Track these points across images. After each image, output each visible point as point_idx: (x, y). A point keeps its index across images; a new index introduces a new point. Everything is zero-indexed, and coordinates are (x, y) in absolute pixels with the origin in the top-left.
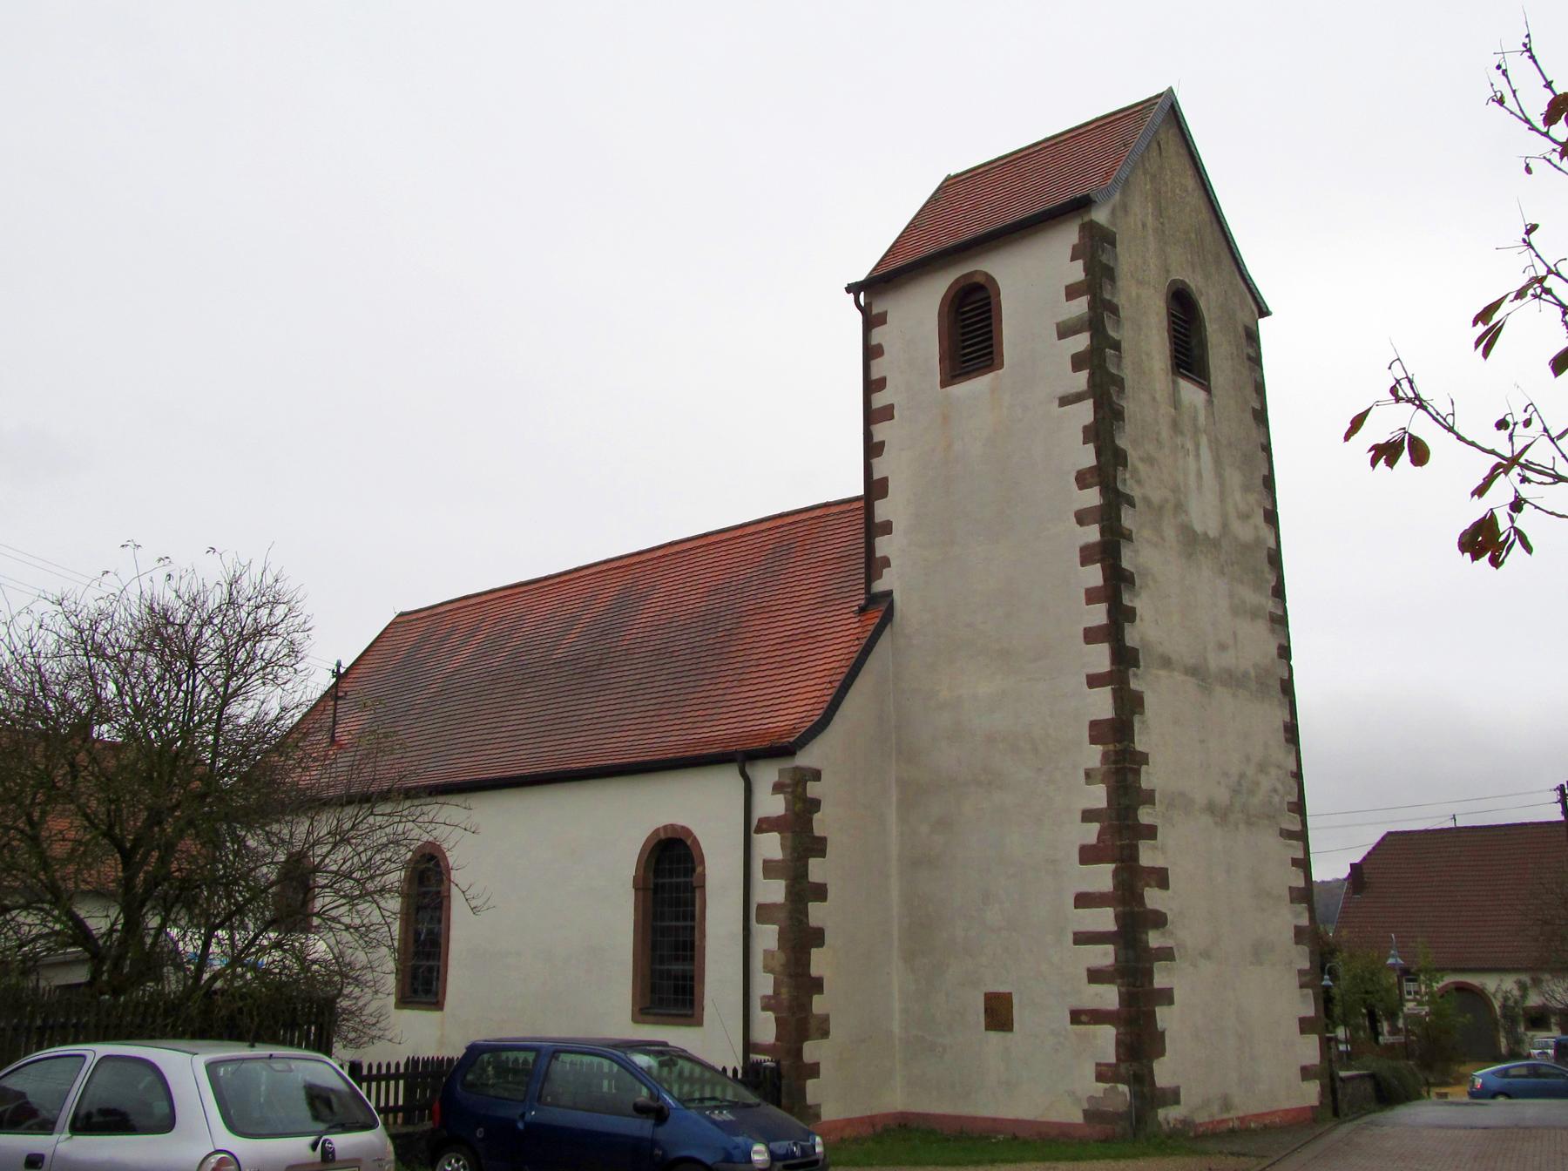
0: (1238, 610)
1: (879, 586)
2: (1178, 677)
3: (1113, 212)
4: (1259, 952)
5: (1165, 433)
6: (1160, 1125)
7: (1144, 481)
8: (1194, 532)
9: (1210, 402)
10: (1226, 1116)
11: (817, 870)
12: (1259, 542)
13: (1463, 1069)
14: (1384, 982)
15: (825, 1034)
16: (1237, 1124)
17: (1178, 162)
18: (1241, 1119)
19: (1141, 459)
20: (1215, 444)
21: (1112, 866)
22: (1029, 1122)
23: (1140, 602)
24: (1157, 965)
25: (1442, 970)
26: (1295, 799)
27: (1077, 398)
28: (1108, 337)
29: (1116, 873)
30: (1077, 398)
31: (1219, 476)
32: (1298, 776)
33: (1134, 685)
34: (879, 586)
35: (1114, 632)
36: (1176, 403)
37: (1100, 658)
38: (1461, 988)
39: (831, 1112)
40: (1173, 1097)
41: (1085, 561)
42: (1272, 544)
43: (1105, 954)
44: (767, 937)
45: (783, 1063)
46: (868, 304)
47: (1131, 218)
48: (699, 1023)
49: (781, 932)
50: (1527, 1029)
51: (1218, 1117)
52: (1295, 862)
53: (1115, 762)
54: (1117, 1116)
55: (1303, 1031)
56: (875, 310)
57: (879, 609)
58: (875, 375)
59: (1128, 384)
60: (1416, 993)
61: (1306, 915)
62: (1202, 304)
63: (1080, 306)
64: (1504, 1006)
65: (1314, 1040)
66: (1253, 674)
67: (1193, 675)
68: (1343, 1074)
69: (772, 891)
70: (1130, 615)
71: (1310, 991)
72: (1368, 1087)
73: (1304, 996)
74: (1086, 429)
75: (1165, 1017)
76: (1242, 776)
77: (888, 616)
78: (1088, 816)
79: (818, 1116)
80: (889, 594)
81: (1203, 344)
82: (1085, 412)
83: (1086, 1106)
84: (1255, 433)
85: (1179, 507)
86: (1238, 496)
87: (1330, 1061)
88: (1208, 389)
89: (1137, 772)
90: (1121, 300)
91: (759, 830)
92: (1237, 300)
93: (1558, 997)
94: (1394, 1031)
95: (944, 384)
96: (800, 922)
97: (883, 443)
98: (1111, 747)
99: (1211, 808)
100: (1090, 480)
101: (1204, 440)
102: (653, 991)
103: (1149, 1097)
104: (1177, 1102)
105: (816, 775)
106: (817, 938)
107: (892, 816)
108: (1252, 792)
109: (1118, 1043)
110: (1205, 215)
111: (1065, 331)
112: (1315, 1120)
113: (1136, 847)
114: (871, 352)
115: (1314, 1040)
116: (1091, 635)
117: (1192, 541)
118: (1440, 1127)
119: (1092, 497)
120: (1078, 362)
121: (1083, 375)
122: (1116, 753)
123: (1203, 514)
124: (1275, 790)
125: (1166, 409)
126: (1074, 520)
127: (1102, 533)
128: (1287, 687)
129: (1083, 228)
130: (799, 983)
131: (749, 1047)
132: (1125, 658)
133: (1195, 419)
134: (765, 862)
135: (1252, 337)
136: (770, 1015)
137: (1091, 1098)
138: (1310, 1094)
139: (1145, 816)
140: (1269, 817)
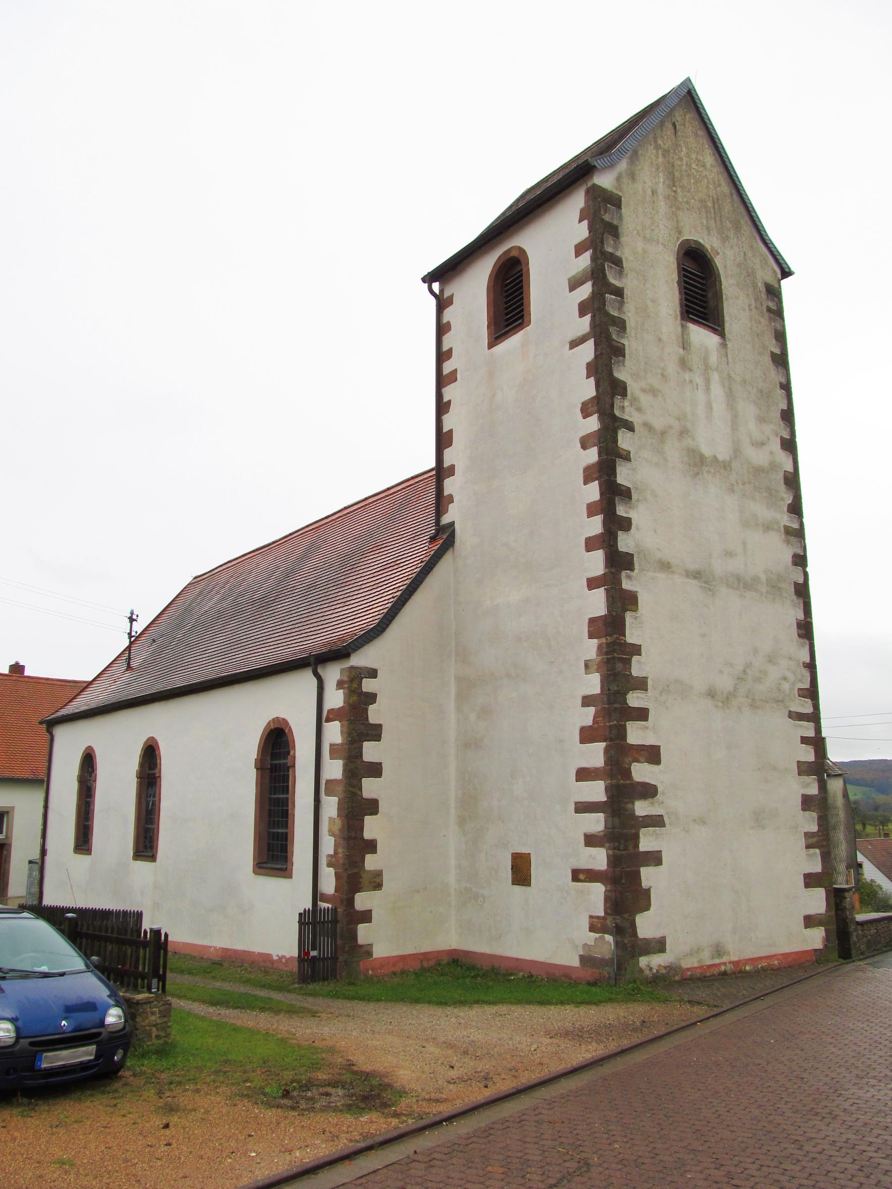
1: (446, 520)
2: (679, 579)
3: (619, 179)
4: (760, 818)
5: (672, 368)
6: (641, 970)
7: (640, 407)
9: (724, 345)
10: (717, 961)
12: (773, 466)
15: (378, 886)
16: (729, 967)
18: (736, 963)
19: (643, 390)
20: (728, 381)
22: (541, 963)
24: (643, 831)
26: (807, 685)
27: (582, 340)
28: (609, 285)
29: (606, 751)
30: (582, 340)
32: (811, 666)
33: (626, 585)
34: (446, 520)
36: (685, 344)
37: (596, 563)
39: (380, 951)
41: (587, 480)
42: (790, 469)
43: (598, 821)
44: (331, 806)
45: (340, 910)
46: (442, 291)
48: (290, 876)
49: (339, 803)
53: (607, 653)
55: (807, 885)
57: (444, 538)
59: (631, 323)
61: (816, 785)
62: (718, 262)
63: (585, 260)
66: (763, 577)
67: (695, 578)
69: (334, 769)
70: (626, 524)
71: (817, 851)
75: (648, 876)
76: (749, 665)
78: (587, 701)
79: (369, 954)
80: (452, 524)
82: (588, 351)
83: (582, 953)
84: (775, 376)
85: (684, 433)
86: (752, 425)
88: (721, 334)
89: (628, 662)
92: (757, 261)
95: (491, 345)
97: (449, 402)
98: (604, 640)
99: (711, 694)
100: (591, 410)
101: (715, 377)
102: (269, 850)
103: (631, 946)
105: (373, 673)
106: (372, 807)
107: (451, 706)
109: (607, 899)
111: (574, 285)
112: (818, 962)
114: (442, 329)
117: (698, 463)
119: (593, 424)
121: (588, 318)
122: (608, 644)
123: (712, 439)
124: (785, 679)
126: (579, 445)
128: (802, 591)
129: (587, 192)
130: (355, 846)
132: (619, 562)
133: (705, 359)
134: (331, 745)
135: (774, 293)
136: (331, 870)
137: (585, 945)
138: (816, 938)
139: (634, 700)
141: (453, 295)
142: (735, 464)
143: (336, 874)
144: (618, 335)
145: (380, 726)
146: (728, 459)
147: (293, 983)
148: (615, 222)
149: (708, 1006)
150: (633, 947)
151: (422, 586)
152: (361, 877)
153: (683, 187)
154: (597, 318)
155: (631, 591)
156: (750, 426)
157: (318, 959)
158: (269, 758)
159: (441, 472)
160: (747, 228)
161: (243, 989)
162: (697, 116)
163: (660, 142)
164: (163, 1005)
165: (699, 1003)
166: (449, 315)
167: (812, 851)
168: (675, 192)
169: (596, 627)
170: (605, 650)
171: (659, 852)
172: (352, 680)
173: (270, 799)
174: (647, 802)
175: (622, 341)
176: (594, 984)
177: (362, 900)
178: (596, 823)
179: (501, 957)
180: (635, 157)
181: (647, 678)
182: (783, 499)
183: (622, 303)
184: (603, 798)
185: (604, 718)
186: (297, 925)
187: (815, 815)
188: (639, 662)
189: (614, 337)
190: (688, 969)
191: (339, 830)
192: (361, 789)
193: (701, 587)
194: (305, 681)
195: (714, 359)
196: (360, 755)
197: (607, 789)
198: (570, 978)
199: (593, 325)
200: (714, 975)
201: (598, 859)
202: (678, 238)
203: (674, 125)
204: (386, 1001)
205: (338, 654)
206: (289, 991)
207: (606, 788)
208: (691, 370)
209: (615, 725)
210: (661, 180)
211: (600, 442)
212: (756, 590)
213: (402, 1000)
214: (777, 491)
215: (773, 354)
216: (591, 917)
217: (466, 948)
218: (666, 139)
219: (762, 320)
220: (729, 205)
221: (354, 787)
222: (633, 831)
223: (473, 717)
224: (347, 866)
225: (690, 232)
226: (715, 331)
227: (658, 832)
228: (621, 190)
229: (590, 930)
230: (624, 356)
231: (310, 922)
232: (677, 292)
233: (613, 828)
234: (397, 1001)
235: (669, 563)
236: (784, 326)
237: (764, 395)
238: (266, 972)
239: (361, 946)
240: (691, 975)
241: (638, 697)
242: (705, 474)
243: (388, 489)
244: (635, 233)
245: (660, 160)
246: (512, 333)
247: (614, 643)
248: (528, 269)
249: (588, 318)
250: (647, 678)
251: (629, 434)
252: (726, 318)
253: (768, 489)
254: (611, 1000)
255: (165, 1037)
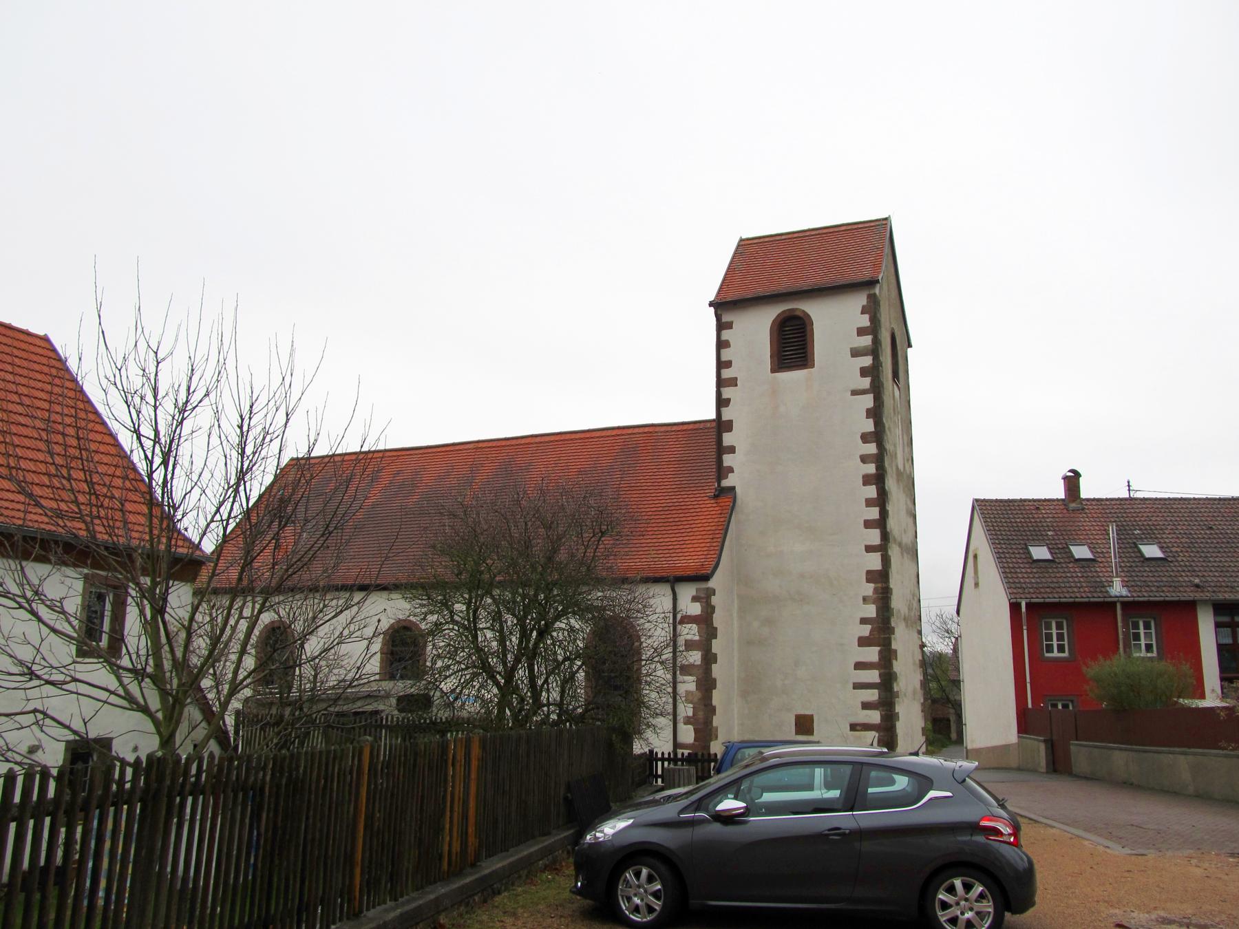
1: (725, 483)
29: (880, 652)
178: (873, 695)
184: (878, 680)
223: (756, 624)
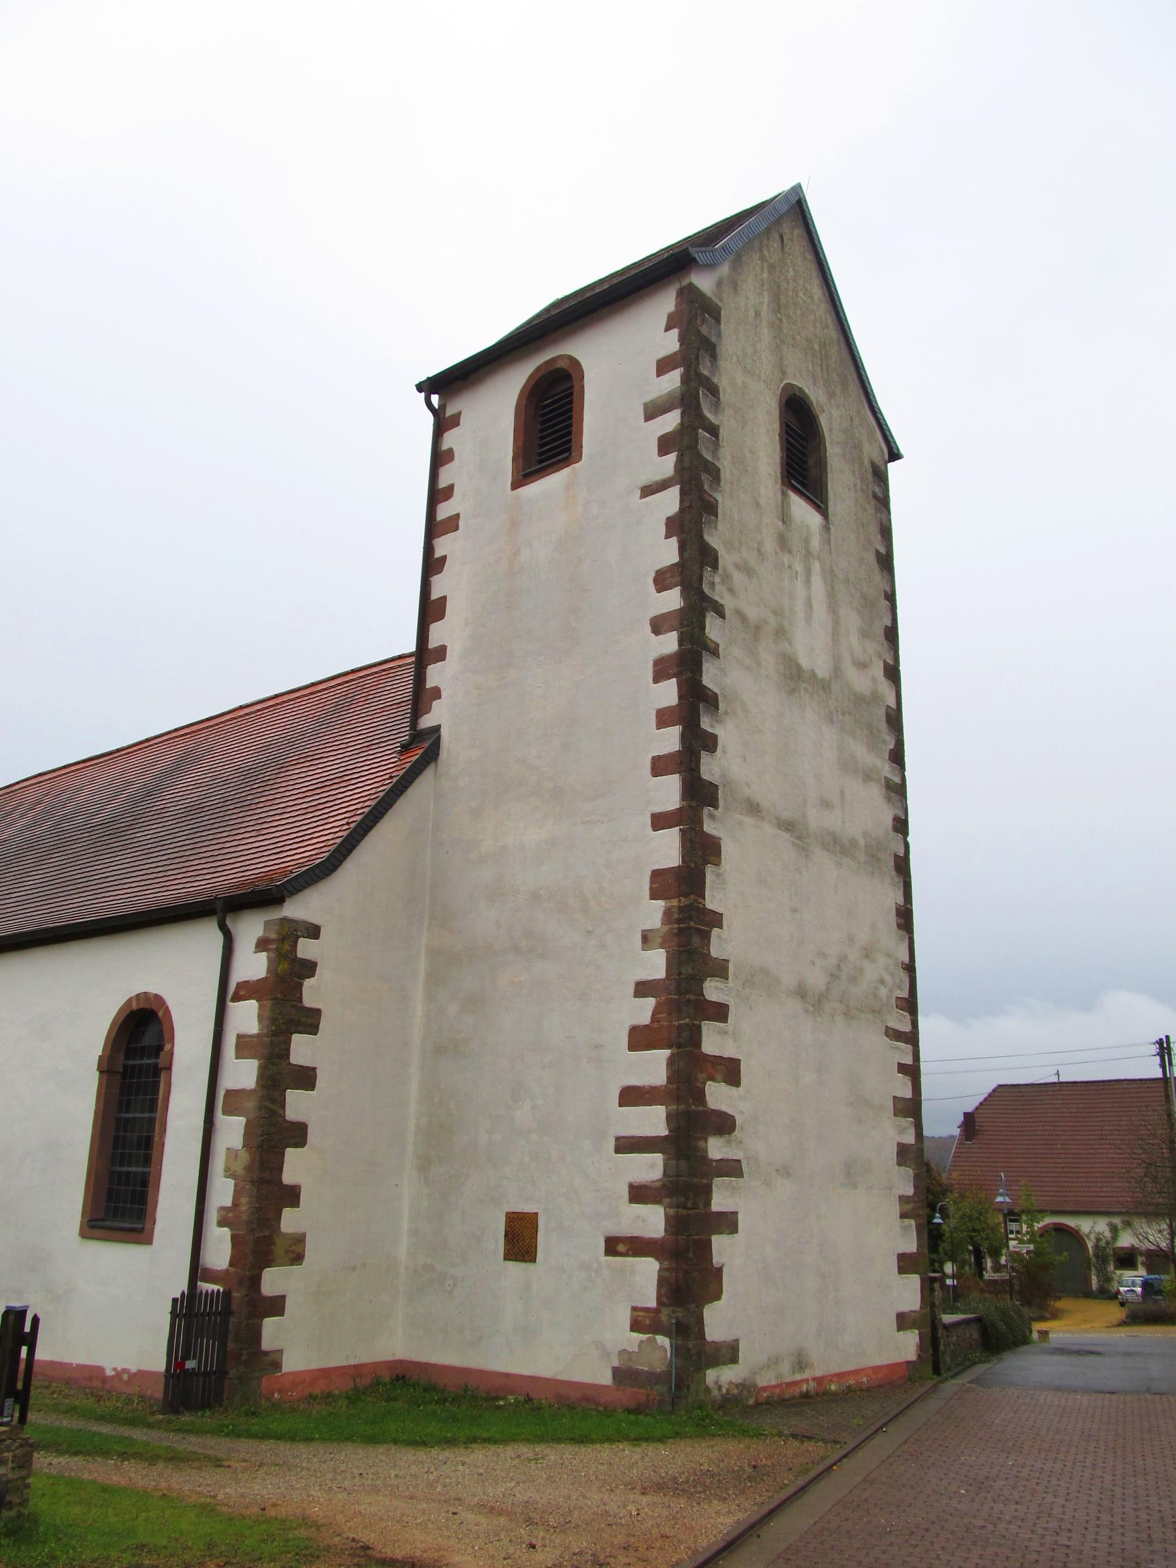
0: (847, 766)
1: (426, 722)
2: (769, 829)
3: (719, 284)
4: (852, 1173)
5: (770, 545)
6: (708, 1390)
7: (738, 590)
8: (799, 666)
9: (826, 528)
10: (798, 1377)
11: (302, 1049)
12: (876, 697)
13: (1059, 1304)
14: (990, 1222)
15: (298, 1258)
17: (797, 246)
18: (819, 1380)
19: (737, 566)
20: (830, 575)
21: (667, 1053)
23: (725, 731)
24: (717, 1181)
25: (1042, 1211)
29: (671, 1062)
31: (833, 608)
32: (910, 968)
33: (709, 827)
34: (426, 722)
35: (689, 761)
36: (785, 517)
37: (668, 792)
38: (1060, 1229)
39: (294, 1361)
40: (729, 1353)
41: (658, 677)
42: (892, 702)
43: (653, 1166)
44: (232, 1131)
45: (235, 1294)
46: (443, 406)
47: (745, 305)
48: (149, 1241)
49: (248, 1126)
50: (1116, 1268)
51: (789, 1379)
52: (902, 1068)
53: (679, 921)
54: (652, 1378)
55: (902, 1270)
56: (450, 412)
57: (423, 748)
58: (442, 483)
59: (726, 475)
60: (1018, 1232)
61: (912, 1131)
62: (823, 420)
63: (673, 380)
64: (1096, 1247)
65: (914, 1280)
66: (862, 842)
67: (787, 830)
68: (947, 1318)
69: (242, 1074)
70: (710, 743)
71: (913, 1222)
72: (974, 1333)
73: (905, 1228)
74: (670, 522)
75: (722, 1247)
76: (843, 958)
77: (432, 755)
78: (643, 989)
79: (277, 1365)
80: (437, 729)
81: (822, 464)
82: (670, 502)
83: (616, 1364)
84: (878, 578)
85: (781, 633)
87: (933, 1305)
89: (706, 936)
90: (723, 382)
91: (237, 998)
93: (1151, 1238)
94: (997, 1268)
95: (516, 485)
96: (273, 1113)
98: (675, 902)
99: (801, 993)
101: (816, 567)
102: (109, 1199)
103: (696, 1352)
104: (734, 1360)
105: (314, 932)
106: (298, 1134)
107: (418, 991)
108: (853, 980)
109: (661, 1282)
110: (833, 333)
111: (652, 411)
113: (699, 1028)
114: (440, 458)
115: (914, 1280)
116: (660, 766)
117: (794, 676)
118: (1058, 1389)
120: (665, 445)
121: (672, 458)
122: (681, 909)
123: (812, 648)
124: (882, 982)
125: (771, 521)
127: (681, 642)
128: (902, 866)
129: (680, 293)
131: (197, 1271)
132: (700, 794)
133: (807, 541)
134: (239, 1037)
135: (881, 477)
138: (907, 1345)
139: (713, 991)
140: (873, 1011)
141: (460, 414)
142: (835, 687)
143: (233, 1237)
144: (711, 486)
145: (318, 1011)
146: (827, 677)
147: (153, 1413)
148: (713, 339)
149: (825, 1441)
150: (699, 1355)
151: (390, 812)
152: (274, 1244)
153: (788, 316)
154: (686, 460)
155: (713, 837)
156: (853, 641)
157: (197, 1374)
158: (121, 1056)
159: (425, 654)
160: (854, 387)
161: (77, 1424)
162: (805, 234)
163: (765, 253)
164: (21, 1446)
165: (810, 1438)
166: (450, 439)
167: (907, 1221)
168: (780, 320)
169: (662, 883)
170: (676, 916)
171: (735, 1214)
172: (282, 940)
173: (118, 1120)
174: (722, 1140)
175: (716, 495)
176: (637, 1410)
177: (273, 1281)
178: (650, 1167)
179: (482, 1372)
180: (737, 263)
181: (728, 961)
182: (884, 742)
183: (716, 445)
184: (662, 1130)
185: (669, 1014)
186: (169, 1316)
187: (911, 1172)
188: (719, 937)
189: (706, 487)
190: (764, 1389)
191: (245, 1168)
192: (283, 1106)
193: (794, 844)
194: (203, 939)
195: (816, 543)
196: (286, 1054)
197: (669, 1117)
198: (597, 1404)
199: (680, 466)
200: (794, 1398)
201: (652, 1221)
202: (782, 380)
203: (781, 237)
204: (323, 1440)
205: (264, 896)
206: (150, 1426)
207: (667, 1116)
208: (790, 552)
209: (687, 1024)
210: (766, 300)
211: (682, 625)
212: (854, 858)
213: (349, 1439)
214: (879, 731)
215: (878, 553)
216: (634, 1309)
217: (422, 1358)
218: (772, 251)
219: (868, 507)
220: (836, 353)
221: (274, 1102)
222: (705, 1181)
223: (453, 1008)
224: (255, 1226)
225: (795, 376)
226: (817, 507)
227: (734, 1184)
228: (721, 300)
229: (632, 1330)
230: (717, 516)
231: (190, 1315)
232: (778, 448)
233: (678, 1176)
234: (338, 1440)
235: (758, 805)
236: (890, 520)
237: (867, 604)
238: (99, 1398)
239: (266, 1353)
240: (768, 1397)
241: (717, 988)
242: (802, 692)
243: (313, 684)
244: (735, 359)
245: (765, 275)
246: (550, 470)
247: (690, 907)
248: (582, 387)
249: (672, 458)
250: (728, 961)
251: (719, 621)
252: (831, 495)
253: (869, 726)
254: (678, 1435)
255: (21, 1504)
